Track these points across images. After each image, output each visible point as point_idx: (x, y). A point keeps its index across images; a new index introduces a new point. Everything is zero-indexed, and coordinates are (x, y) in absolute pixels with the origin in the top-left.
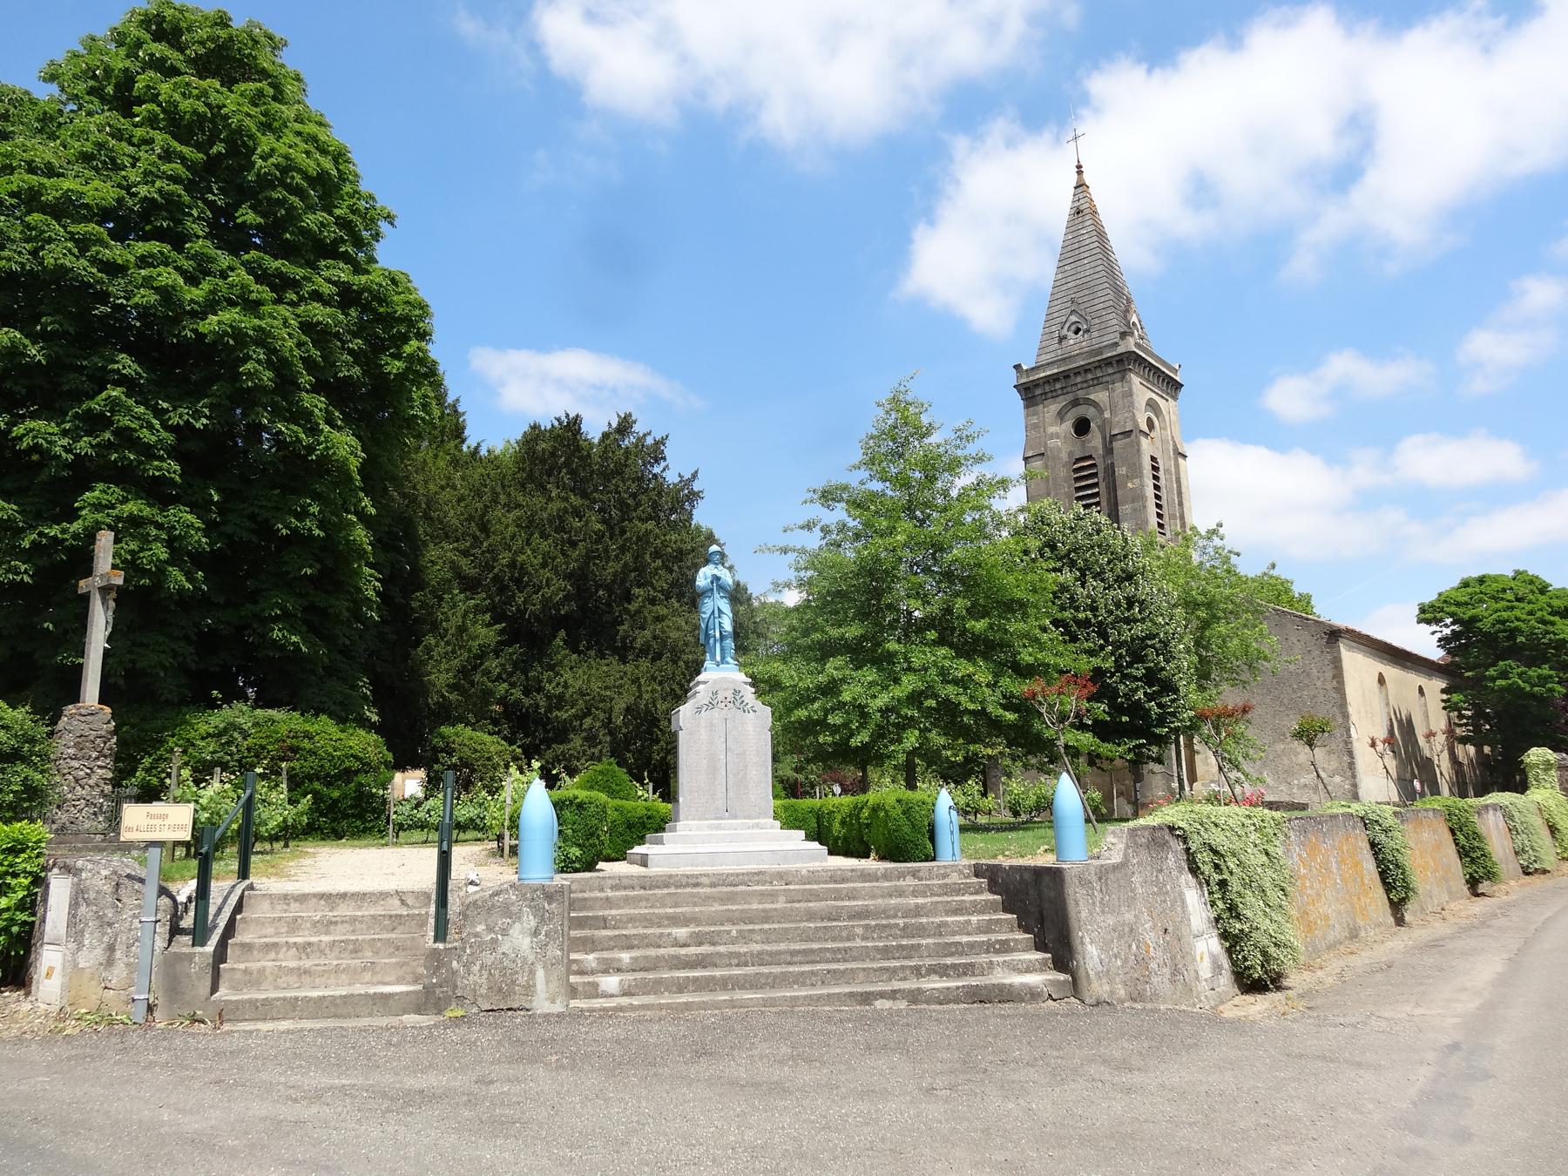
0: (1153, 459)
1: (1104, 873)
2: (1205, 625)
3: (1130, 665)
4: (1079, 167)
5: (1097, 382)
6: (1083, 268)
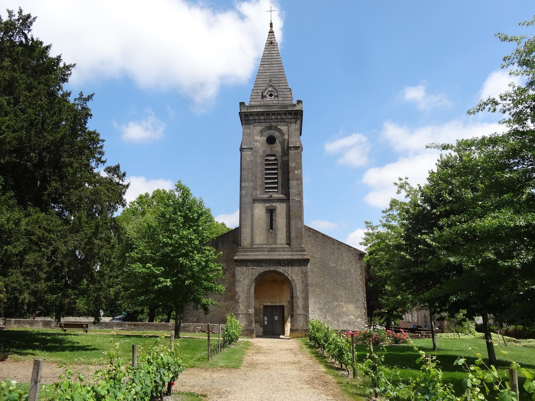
4: (271, 24)
5: (283, 121)
6: (274, 68)
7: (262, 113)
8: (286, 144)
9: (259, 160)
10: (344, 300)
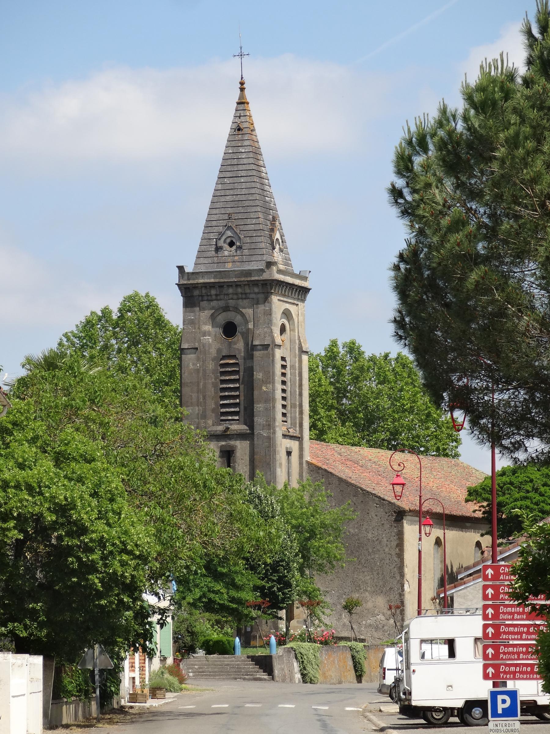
0: (283, 359)
1: (279, 657)
2: (308, 539)
3: (271, 575)
4: (242, 84)
5: (245, 296)
7: (211, 285)
8: (250, 343)
9: (211, 366)
10: (369, 589)
